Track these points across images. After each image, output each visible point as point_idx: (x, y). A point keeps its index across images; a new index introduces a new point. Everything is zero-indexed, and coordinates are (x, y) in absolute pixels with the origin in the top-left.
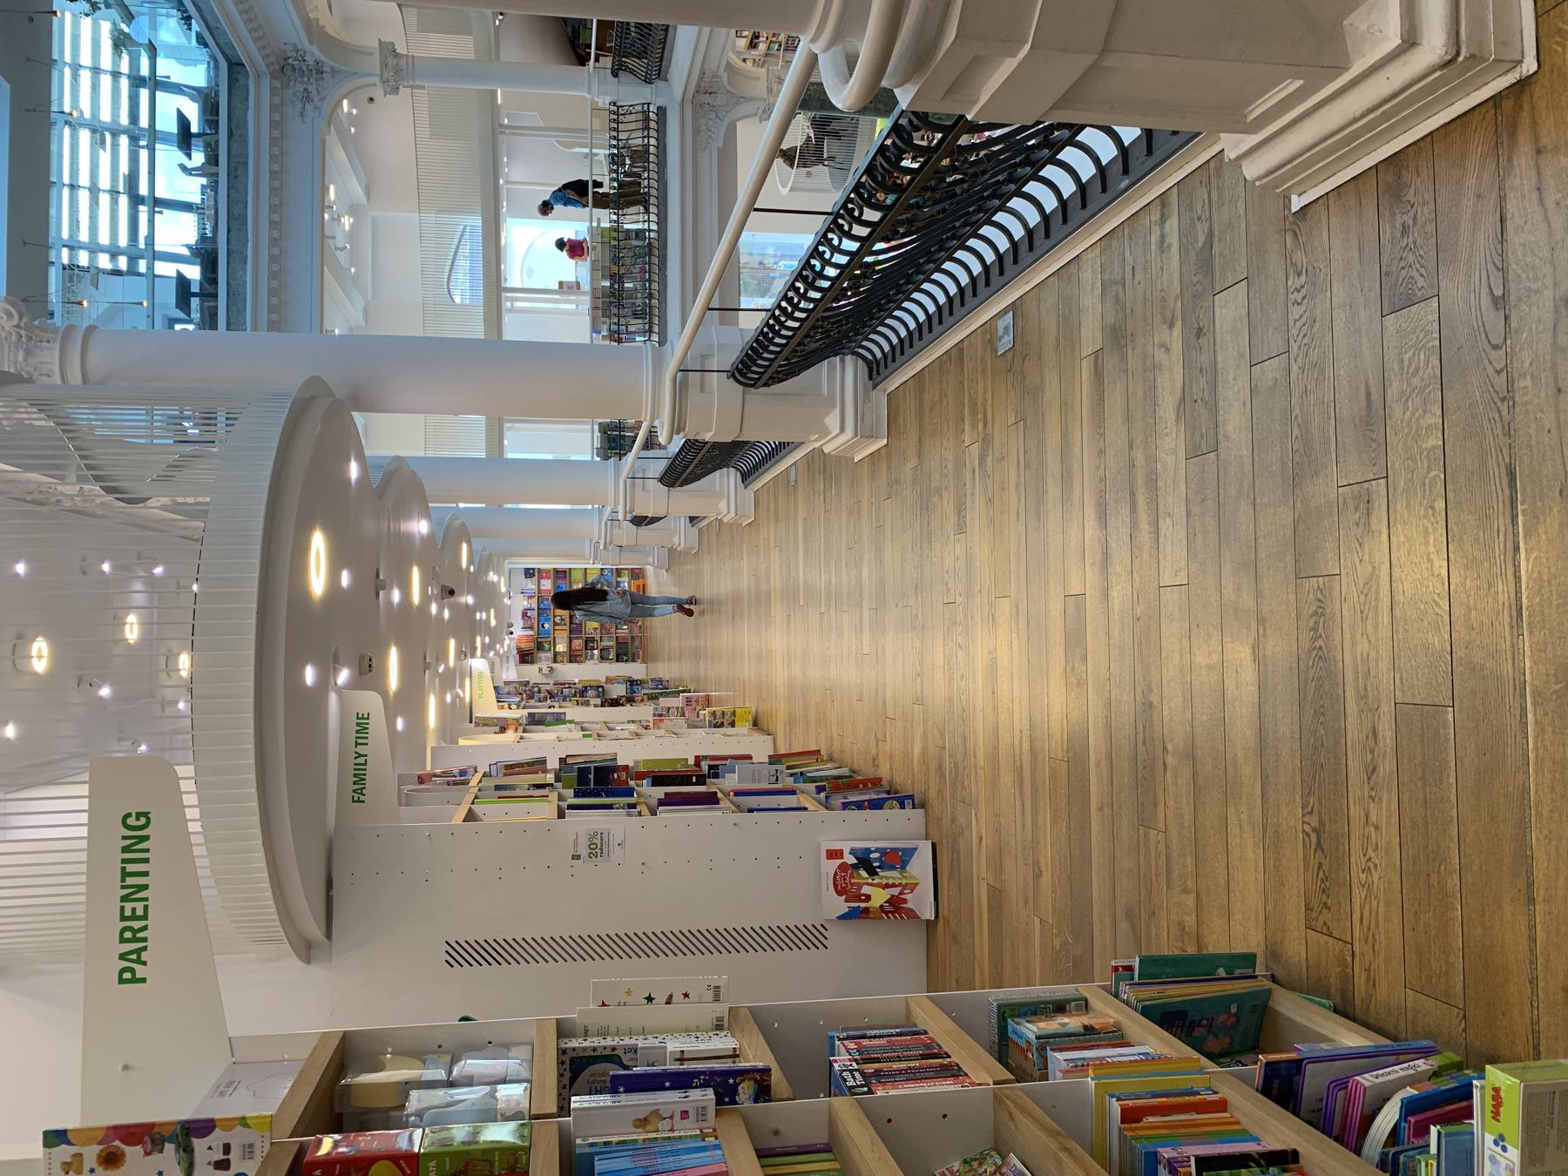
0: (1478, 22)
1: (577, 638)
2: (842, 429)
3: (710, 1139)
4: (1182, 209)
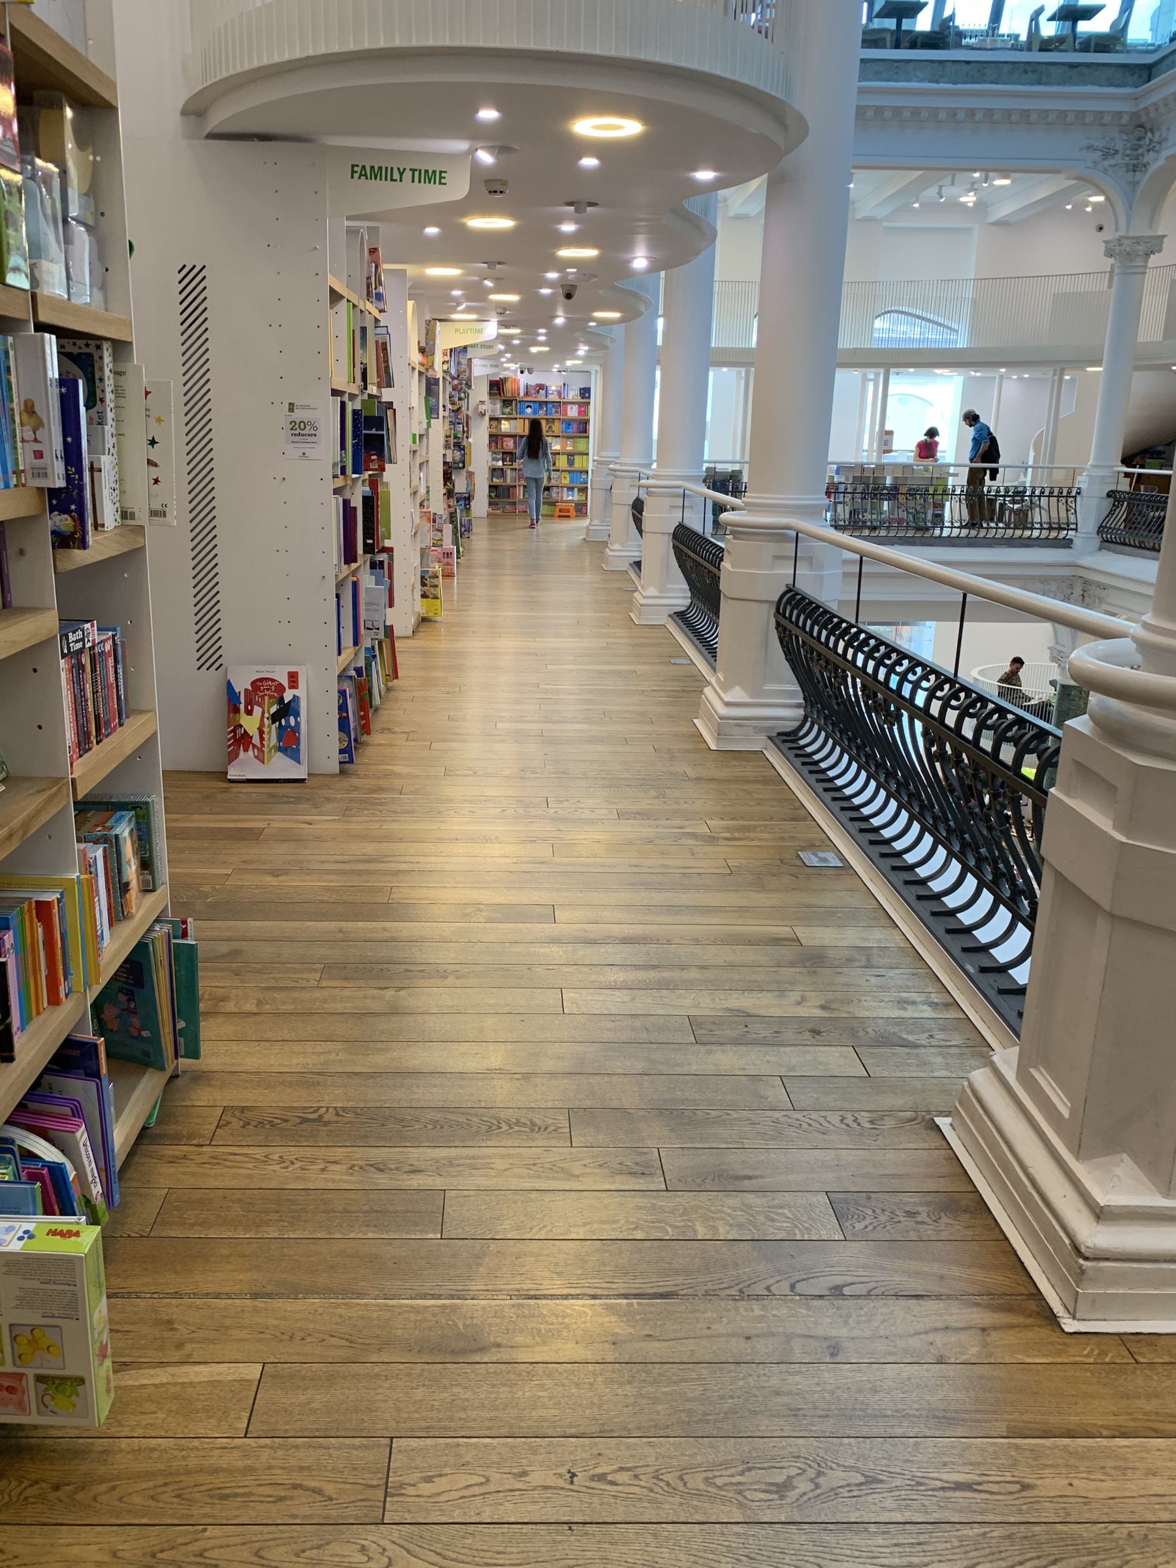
0: (1116, 1279)
1: (515, 443)
2: (728, 704)
3: (15, 480)
4: (941, 1022)
